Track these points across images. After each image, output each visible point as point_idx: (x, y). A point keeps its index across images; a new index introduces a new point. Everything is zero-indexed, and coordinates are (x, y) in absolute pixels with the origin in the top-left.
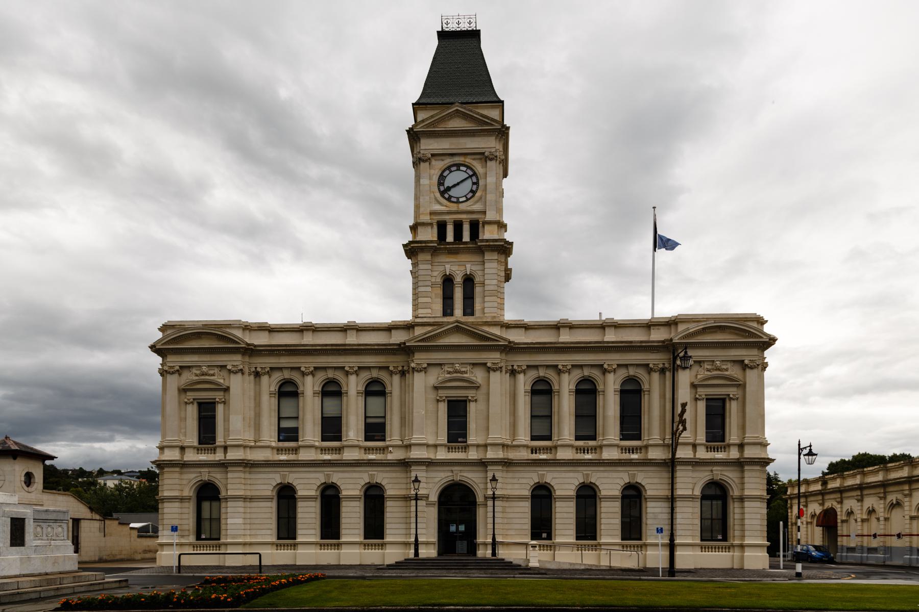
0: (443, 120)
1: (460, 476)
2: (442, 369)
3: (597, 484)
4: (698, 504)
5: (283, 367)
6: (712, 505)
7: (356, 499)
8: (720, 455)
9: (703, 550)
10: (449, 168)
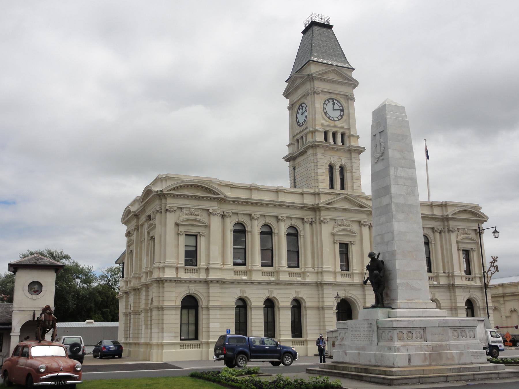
0: (326, 73)
1: (350, 293)
2: (182, 211)
3: (249, 297)
4: (179, 312)
5: (238, 213)
6: (239, 314)
7: (172, 309)
8: (193, 276)
9: (182, 347)
10: (328, 100)
